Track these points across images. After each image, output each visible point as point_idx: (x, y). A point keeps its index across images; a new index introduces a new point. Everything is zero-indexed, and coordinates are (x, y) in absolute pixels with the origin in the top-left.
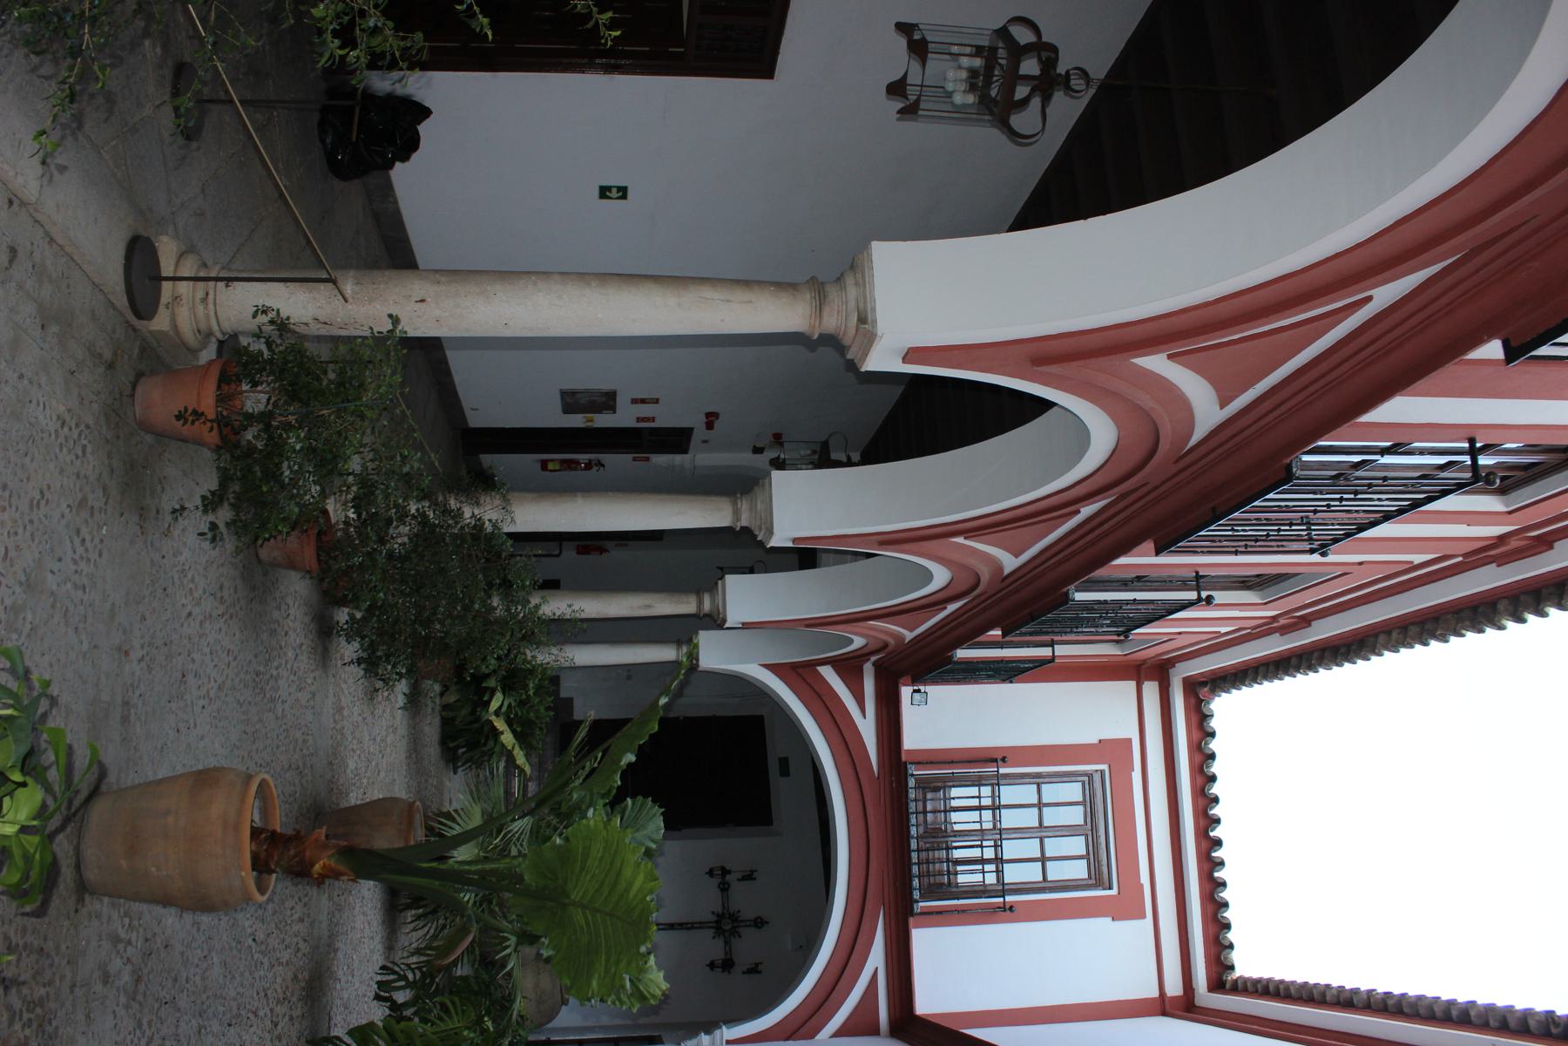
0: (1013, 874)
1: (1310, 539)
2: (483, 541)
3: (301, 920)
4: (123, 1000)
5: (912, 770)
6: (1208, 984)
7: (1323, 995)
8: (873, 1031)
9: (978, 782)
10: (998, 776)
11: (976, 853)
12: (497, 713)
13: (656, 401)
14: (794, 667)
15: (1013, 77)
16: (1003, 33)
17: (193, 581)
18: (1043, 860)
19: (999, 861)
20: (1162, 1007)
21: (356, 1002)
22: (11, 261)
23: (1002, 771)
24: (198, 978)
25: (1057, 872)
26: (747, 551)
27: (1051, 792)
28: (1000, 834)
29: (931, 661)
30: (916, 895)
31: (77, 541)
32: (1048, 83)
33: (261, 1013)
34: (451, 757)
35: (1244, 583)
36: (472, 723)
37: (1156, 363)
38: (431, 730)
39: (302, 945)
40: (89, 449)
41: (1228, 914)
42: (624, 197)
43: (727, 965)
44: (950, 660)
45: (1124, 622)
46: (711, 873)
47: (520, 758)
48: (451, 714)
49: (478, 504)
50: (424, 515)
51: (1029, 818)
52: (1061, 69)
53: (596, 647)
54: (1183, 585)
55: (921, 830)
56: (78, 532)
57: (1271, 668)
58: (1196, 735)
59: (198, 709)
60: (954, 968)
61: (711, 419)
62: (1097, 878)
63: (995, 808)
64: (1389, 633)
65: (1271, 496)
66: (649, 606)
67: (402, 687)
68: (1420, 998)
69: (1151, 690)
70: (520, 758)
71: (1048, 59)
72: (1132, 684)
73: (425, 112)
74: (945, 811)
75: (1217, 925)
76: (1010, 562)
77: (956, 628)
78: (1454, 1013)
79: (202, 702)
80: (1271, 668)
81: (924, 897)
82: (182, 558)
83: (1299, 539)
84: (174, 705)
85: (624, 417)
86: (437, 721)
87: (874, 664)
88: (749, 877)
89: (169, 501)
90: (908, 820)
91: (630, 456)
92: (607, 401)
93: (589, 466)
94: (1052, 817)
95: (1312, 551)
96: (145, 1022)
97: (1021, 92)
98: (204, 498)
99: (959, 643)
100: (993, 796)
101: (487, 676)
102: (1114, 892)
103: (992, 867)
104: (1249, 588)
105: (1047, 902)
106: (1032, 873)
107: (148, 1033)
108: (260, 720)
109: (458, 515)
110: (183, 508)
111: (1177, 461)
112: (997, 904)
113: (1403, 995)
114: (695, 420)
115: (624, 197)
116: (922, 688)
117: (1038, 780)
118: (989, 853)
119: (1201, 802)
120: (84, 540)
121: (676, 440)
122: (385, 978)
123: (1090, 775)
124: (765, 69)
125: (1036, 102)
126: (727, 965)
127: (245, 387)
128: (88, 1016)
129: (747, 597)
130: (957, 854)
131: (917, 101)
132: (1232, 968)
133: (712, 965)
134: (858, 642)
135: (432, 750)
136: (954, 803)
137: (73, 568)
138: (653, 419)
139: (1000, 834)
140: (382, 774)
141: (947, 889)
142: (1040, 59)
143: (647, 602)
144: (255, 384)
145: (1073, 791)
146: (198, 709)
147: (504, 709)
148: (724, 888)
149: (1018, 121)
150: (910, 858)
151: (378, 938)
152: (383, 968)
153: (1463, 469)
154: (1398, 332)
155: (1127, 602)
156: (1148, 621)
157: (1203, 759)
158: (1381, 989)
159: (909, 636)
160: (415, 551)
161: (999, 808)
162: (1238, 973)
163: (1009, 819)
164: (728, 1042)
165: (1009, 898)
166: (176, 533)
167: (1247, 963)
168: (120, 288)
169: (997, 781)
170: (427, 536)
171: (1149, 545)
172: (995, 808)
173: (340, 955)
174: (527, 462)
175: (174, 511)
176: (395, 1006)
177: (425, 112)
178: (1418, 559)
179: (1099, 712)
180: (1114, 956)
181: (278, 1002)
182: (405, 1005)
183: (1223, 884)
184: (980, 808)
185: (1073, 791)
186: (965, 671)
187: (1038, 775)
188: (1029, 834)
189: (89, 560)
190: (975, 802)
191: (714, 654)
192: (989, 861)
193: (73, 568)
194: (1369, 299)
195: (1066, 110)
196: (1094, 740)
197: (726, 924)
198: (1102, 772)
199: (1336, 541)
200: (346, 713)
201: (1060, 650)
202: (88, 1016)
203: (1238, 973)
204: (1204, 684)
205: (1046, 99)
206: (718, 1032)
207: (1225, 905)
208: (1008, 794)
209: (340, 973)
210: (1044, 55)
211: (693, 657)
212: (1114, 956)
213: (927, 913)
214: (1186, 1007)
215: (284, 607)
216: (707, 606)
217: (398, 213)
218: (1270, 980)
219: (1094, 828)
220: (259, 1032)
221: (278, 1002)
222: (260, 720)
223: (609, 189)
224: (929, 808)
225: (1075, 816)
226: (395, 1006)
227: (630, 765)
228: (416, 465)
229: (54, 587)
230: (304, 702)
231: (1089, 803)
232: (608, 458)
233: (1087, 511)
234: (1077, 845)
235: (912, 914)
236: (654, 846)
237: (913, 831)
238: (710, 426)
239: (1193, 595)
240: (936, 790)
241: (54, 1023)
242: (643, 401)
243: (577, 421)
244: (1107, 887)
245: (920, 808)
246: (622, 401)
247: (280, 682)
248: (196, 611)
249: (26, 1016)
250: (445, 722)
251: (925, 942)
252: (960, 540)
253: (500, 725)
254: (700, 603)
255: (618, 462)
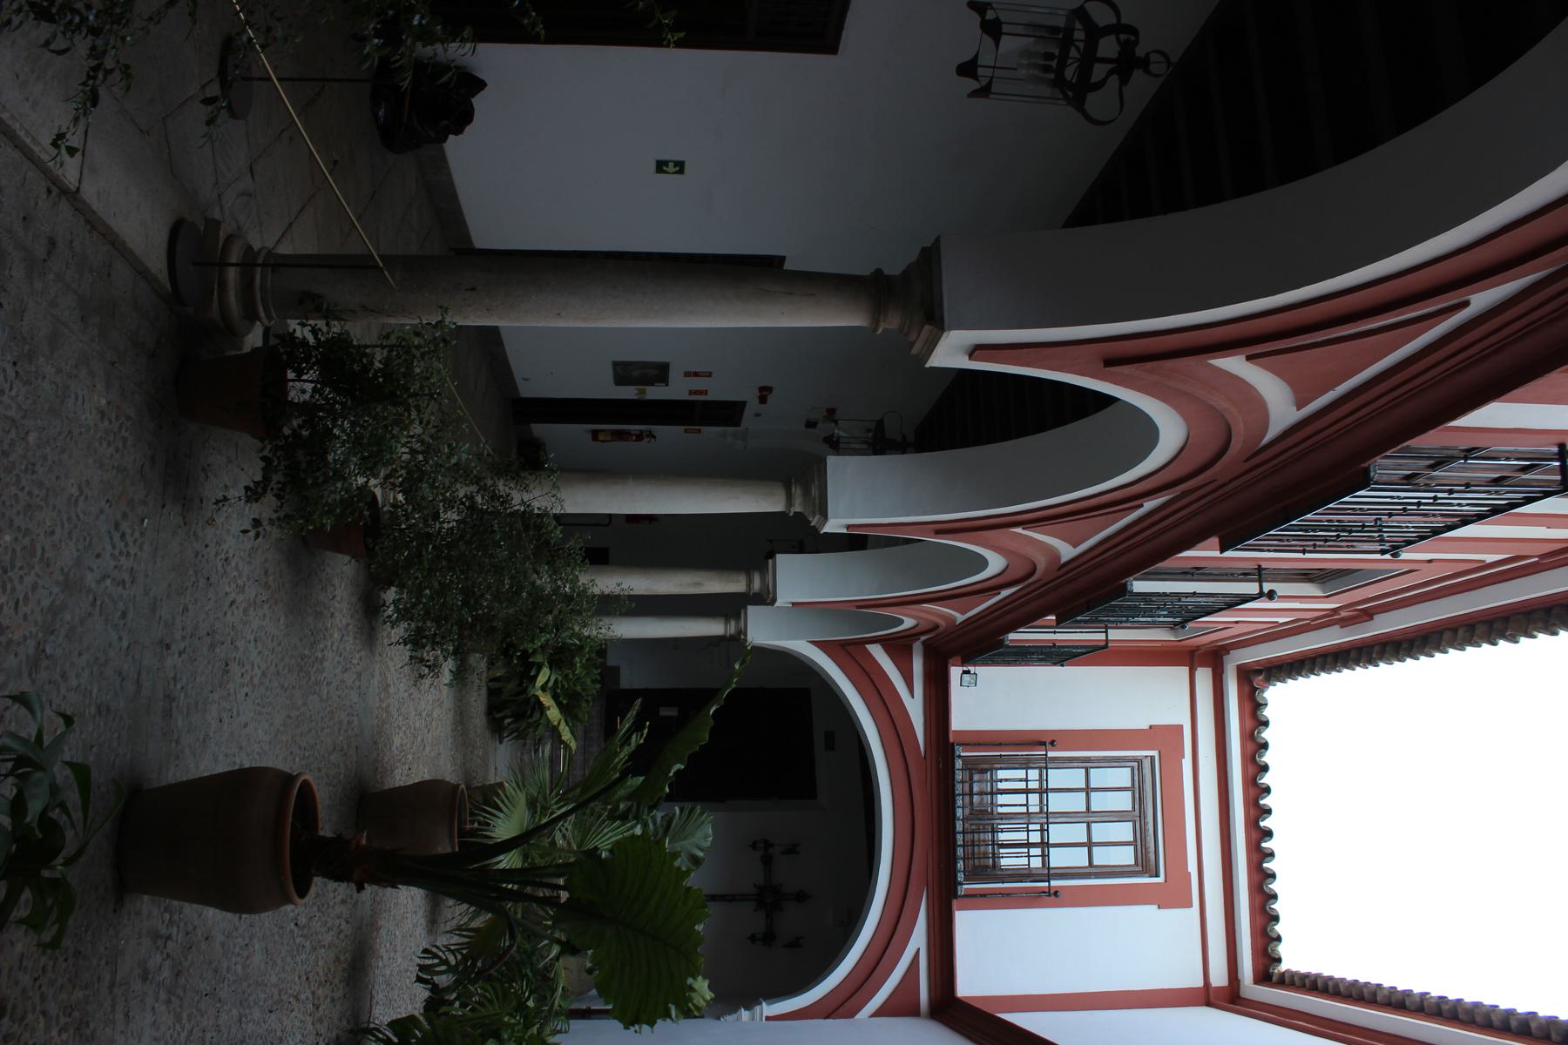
0: (1058, 858)
1: (1382, 541)
2: (530, 521)
3: (343, 902)
4: (163, 996)
5: (961, 752)
6: (1254, 978)
7: (1374, 994)
8: (914, 1012)
9: (1026, 764)
10: (1046, 759)
11: (1022, 836)
12: (543, 688)
13: (710, 375)
14: (843, 645)
15: (1089, 58)
16: (1080, 13)
17: (237, 568)
18: (1090, 845)
19: (1045, 845)
20: (1206, 997)
21: (398, 996)
22: (49, 253)
23: (1050, 754)
24: (239, 967)
25: (1102, 857)
26: (801, 536)
27: (1099, 777)
28: (1047, 818)
29: (983, 643)
30: (961, 877)
31: (117, 536)
32: (1126, 64)
33: (303, 997)
34: (496, 728)
35: (1306, 576)
36: (518, 694)
37: (1234, 364)
38: (477, 702)
39: (344, 926)
40: (129, 442)
41: (1277, 906)
42: (681, 172)
43: (769, 937)
44: (1001, 644)
45: (1185, 612)
46: (754, 846)
47: (566, 735)
48: (497, 685)
49: (526, 489)
50: (471, 498)
51: (1076, 803)
52: (1140, 51)
53: (641, 617)
54: (1245, 576)
55: (967, 811)
56: (117, 526)
57: (1329, 659)
58: (1249, 724)
59: (241, 697)
60: (997, 953)
61: (764, 393)
62: (1145, 865)
63: (1043, 791)
64: (1455, 631)
65: (1347, 499)
66: (698, 584)
67: (448, 666)
68: (1477, 1005)
69: (1204, 676)
70: (566, 735)
71: (1127, 41)
72: (1185, 670)
73: (480, 85)
74: (992, 793)
75: (1265, 917)
76: (1067, 552)
77: (1007, 612)
78: (1514, 1024)
79: (246, 690)
80: (1329, 659)
81: (968, 879)
82: (225, 547)
83: (1371, 540)
84: (216, 696)
85: (676, 389)
86: (484, 692)
87: (923, 643)
88: (792, 850)
89: (212, 489)
90: (954, 802)
91: (682, 428)
92: (660, 373)
93: (640, 437)
94: (1100, 802)
95: (1383, 552)
96: (185, 1015)
97: (1099, 71)
98: (247, 488)
99: (1013, 627)
100: (1040, 780)
101: (534, 652)
102: (1161, 879)
103: (1037, 851)
104: (1311, 580)
105: (1093, 888)
106: (1078, 858)
107: (188, 1027)
108: (305, 704)
109: (506, 500)
110: (225, 499)
111: (1247, 460)
112: (1041, 889)
113: (1460, 1000)
114: (750, 395)
115: (681, 172)
116: (972, 669)
117: (1087, 764)
118: (1035, 837)
119: (1253, 792)
120: (123, 535)
121: (728, 413)
122: (430, 962)
123: (1139, 761)
124: (832, 49)
125: (1114, 80)
126: (769, 937)
127: (291, 375)
128: (127, 1015)
129: (797, 578)
130: (1002, 837)
131: (989, 85)
132: (1279, 960)
133: (753, 938)
134: (908, 623)
135: (478, 720)
136: (1001, 786)
137: (112, 563)
138: (706, 392)
139: (1047, 818)
140: (428, 749)
141: (990, 871)
142: (1118, 39)
143: (696, 579)
144: (300, 373)
145: (1122, 776)
146: (241, 697)
147: (551, 684)
148: (767, 861)
149: (1093, 101)
150: (954, 814)
151: (421, 912)
152: (425, 951)
153: (1551, 471)
154: (1493, 339)
155: (1187, 595)
156: (1208, 614)
157: (1255, 747)
158: (1435, 993)
159: (960, 618)
160: (461, 537)
161: (1047, 791)
162: (1283, 967)
163: (1056, 803)
164: (768, 1018)
165: (1053, 883)
166: (219, 521)
167: (1294, 957)
168: (165, 273)
169: (1045, 765)
170: (478, 523)
171: (1215, 540)
172: (1043, 791)
173: (383, 932)
174: (577, 433)
175: (217, 502)
176: (435, 988)
177: (480, 85)
178: (1490, 558)
179: (1152, 697)
180: (1161, 944)
181: (320, 984)
182: (448, 989)
183: (1272, 855)
184: (1027, 791)
185: (1122, 776)
186: (1015, 654)
187: (1087, 760)
188: (1078, 810)
189: (128, 554)
190: (1022, 785)
191: (762, 630)
192: (1034, 845)
193: (112, 563)
194: (1466, 304)
195: (1142, 87)
196: (1145, 726)
197: (768, 898)
198: (1152, 758)
199: (1409, 543)
200: (392, 690)
201: (1114, 634)
202: (127, 1015)
203: (1283, 967)
204: (1259, 672)
205: (1124, 80)
206: (757, 1008)
207: (1274, 897)
208: (1057, 778)
209: (383, 951)
210: (1123, 37)
211: (741, 633)
212: (1161, 944)
213: (970, 895)
214: (1230, 999)
215: (330, 589)
216: (757, 585)
217: (452, 184)
218: (1318, 976)
219: (1142, 815)
220: (300, 1016)
221: (320, 984)
222: (305, 704)
223: (666, 163)
224: (976, 789)
225: (1123, 802)
226: (435, 988)
227: (678, 771)
228: (464, 456)
229: (93, 585)
230: (349, 683)
231: (1137, 790)
232: (660, 430)
233: (1149, 505)
234: (1124, 831)
235: (956, 896)
236: (701, 854)
237: (959, 813)
238: (763, 400)
239: (1251, 588)
240: (983, 771)
241: (92, 1026)
242: (696, 374)
243: (629, 393)
244: (1153, 874)
245: (967, 789)
246: (675, 374)
247: (326, 664)
248: (240, 598)
249: (63, 1020)
250: (492, 693)
251: (966, 922)
252: (1019, 530)
253: (546, 700)
254: (750, 582)
255: (668, 434)
